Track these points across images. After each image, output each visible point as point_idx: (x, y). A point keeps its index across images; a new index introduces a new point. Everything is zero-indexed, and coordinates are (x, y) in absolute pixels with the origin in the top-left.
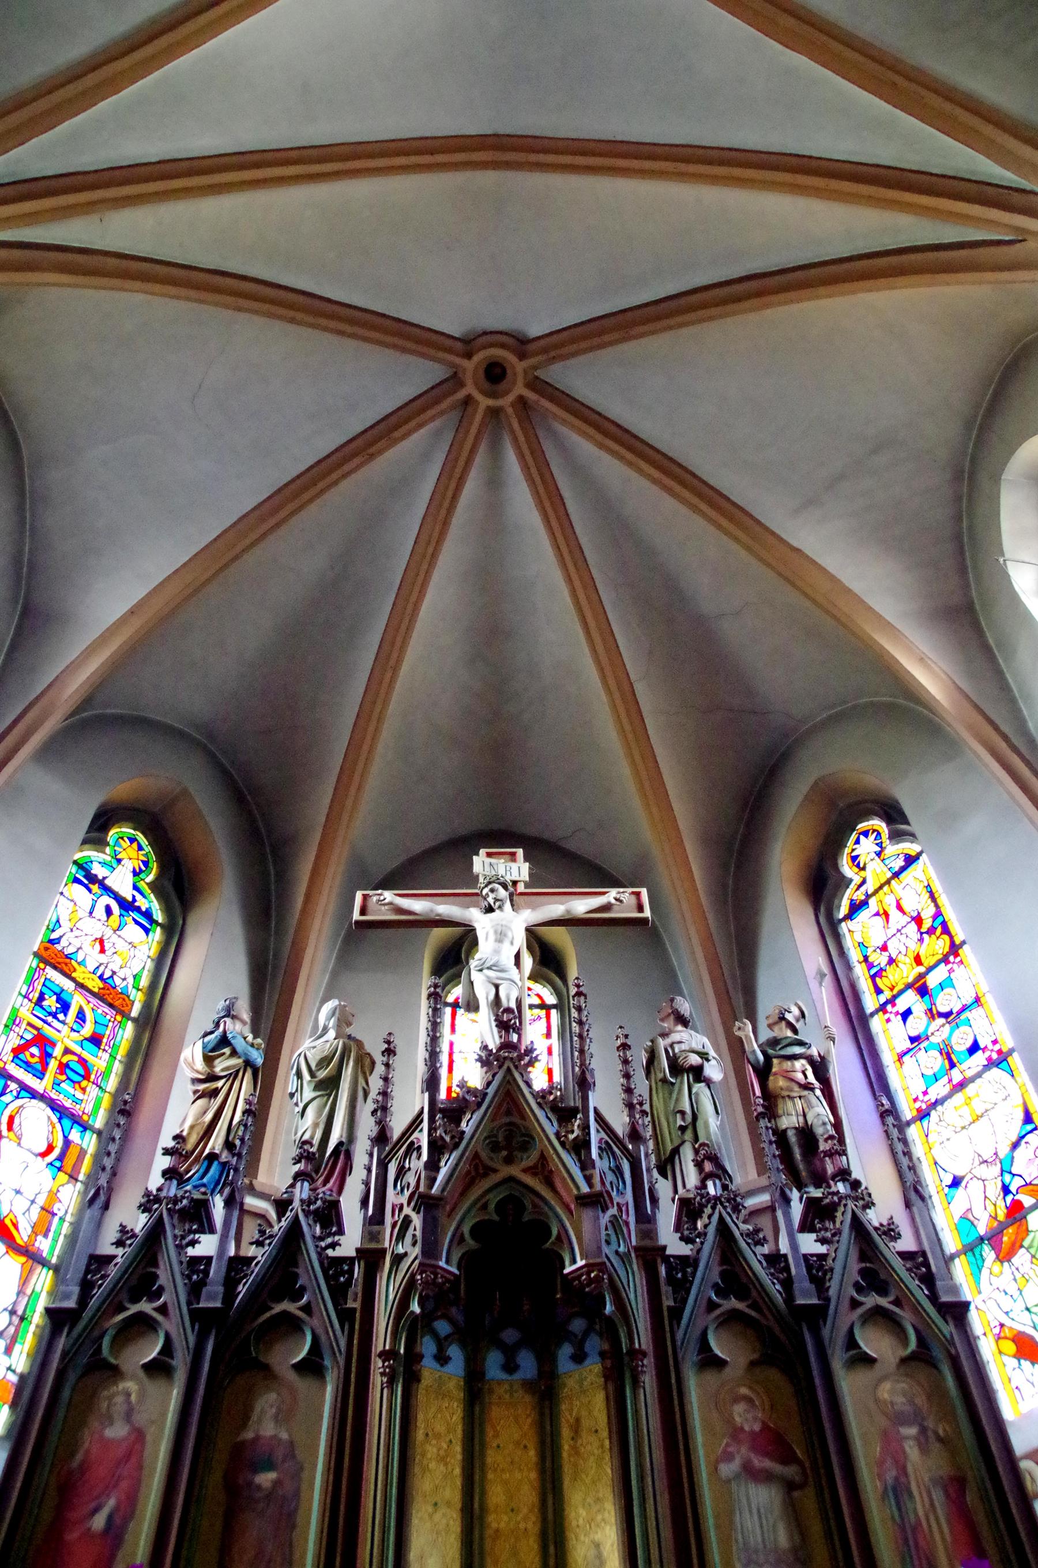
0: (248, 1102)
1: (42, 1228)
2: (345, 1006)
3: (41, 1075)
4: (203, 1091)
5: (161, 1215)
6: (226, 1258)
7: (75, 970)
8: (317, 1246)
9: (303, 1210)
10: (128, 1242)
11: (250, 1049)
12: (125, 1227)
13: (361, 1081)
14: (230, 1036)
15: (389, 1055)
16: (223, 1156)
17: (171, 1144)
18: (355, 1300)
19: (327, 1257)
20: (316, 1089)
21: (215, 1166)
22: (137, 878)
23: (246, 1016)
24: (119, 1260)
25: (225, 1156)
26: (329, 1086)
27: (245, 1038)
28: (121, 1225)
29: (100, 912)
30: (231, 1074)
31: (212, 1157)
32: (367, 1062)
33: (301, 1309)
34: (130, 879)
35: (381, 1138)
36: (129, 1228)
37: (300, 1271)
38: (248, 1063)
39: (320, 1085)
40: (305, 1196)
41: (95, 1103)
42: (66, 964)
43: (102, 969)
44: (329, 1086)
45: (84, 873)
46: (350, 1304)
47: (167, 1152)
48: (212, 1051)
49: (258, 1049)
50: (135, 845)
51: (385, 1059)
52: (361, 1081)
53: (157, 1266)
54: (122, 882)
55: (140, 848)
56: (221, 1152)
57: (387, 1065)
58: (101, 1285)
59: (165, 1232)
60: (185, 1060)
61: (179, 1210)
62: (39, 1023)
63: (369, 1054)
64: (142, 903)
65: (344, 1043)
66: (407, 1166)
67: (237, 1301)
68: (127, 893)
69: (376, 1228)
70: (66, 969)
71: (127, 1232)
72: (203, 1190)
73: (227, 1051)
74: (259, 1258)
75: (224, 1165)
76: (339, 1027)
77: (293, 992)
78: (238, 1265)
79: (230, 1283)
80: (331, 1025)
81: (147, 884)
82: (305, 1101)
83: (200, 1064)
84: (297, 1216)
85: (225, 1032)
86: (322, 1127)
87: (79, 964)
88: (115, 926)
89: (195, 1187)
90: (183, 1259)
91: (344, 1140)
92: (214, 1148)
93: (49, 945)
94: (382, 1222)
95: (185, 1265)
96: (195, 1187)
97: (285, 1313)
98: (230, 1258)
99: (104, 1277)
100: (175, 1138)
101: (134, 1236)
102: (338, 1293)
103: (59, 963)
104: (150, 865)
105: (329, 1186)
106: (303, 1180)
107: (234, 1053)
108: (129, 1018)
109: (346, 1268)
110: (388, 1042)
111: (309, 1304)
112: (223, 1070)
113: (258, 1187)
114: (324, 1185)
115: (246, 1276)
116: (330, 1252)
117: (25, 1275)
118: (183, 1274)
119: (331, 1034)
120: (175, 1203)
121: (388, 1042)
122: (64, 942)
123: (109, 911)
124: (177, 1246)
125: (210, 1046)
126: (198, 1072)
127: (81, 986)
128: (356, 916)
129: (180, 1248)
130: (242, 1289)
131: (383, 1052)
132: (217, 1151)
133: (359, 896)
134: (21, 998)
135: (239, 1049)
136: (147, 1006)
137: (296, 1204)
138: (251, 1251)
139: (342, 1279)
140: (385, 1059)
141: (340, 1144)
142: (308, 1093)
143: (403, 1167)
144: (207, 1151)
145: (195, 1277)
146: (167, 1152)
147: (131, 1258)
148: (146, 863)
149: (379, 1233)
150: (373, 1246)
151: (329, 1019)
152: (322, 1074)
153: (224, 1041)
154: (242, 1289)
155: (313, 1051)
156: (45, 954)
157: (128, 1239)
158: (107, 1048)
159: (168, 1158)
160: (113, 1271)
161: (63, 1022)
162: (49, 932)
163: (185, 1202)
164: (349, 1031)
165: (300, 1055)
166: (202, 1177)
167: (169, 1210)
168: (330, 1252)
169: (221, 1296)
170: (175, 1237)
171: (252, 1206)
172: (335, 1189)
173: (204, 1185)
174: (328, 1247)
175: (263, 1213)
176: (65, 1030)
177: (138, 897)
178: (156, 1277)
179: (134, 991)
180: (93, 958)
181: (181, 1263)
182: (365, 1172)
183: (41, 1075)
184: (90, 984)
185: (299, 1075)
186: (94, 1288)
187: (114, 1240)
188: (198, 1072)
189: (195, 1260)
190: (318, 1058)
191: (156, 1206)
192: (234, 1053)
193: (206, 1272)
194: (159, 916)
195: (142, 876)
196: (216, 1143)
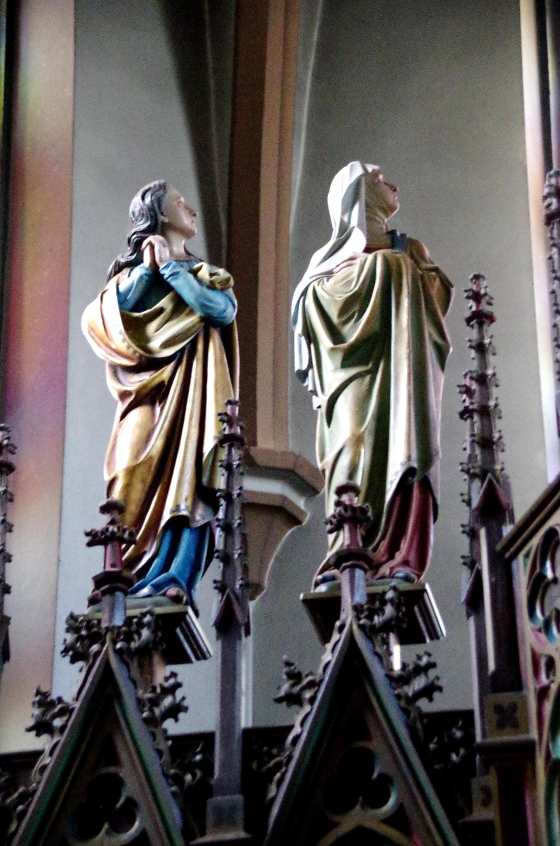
0: (224, 418)
2: (375, 174)
4: (138, 392)
5: (106, 664)
6: (238, 734)
8: (398, 697)
9: (362, 627)
11: (211, 294)
12: (45, 695)
13: (428, 329)
14: (166, 273)
15: (481, 325)
16: (198, 517)
17: (101, 522)
18: (486, 803)
19: (422, 715)
20: (345, 364)
21: (186, 538)
23: (193, 222)
24: (46, 760)
25: (201, 516)
26: (369, 354)
27: (195, 273)
28: (38, 693)
30: (182, 351)
31: (179, 523)
32: (435, 287)
33: (388, 821)
35: (492, 508)
36: (54, 696)
37: (376, 745)
38: (210, 322)
39: (350, 358)
40: (360, 598)
44: (369, 354)
46: (482, 813)
47: (95, 539)
48: (137, 307)
49: (222, 290)
51: (474, 334)
52: (428, 329)
53: (116, 761)
56: (193, 511)
57: (481, 348)
58: (24, 812)
59: (118, 695)
60: (92, 329)
61: (139, 650)
63: (436, 270)
65: (386, 261)
66: (549, 574)
67: (275, 810)
69: (506, 698)
71: (52, 704)
72: (172, 591)
73: (165, 303)
74: (297, 730)
75: (204, 532)
76: (369, 222)
77: (258, 85)
78: (263, 742)
79: (254, 783)
80: (354, 222)
82: (330, 389)
83: (119, 338)
84: (351, 638)
85: (154, 266)
86: (368, 441)
89: (157, 587)
91: (415, 465)
92: (177, 508)
94: (517, 684)
95: (166, 757)
96: (157, 587)
97: (360, 832)
98: (247, 732)
99: (26, 797)
100: (105, 509)
101: (66, 711)
102: (453, 787)
105: (399, 556)
106: (353, 567)
107: (180, 306)
109: (459, 734)
110: (477, 297)
111: (400, 809)
112: (166, 345)
113: (260, 460)
114: (391, 557)
115: (278, 767)
116: (424, 704)
118: (166, 775)
119: (358, 241)
120: (128, 638)
121: (477, 297)
124: (146, 721)
125: (132, 297)
126: (118, 353)
129: (153, 722)
130: (278, 793)
131: (469, 321)
132: (184, 513)
135: (188, 296)
137: (347, 615)
138: (280, 715)
139: (454, 757)
140: (474, 334)
141: (409, 473)
142: (334, 375)
143: (542, 576)
144: (166, 516)
145: (188, 777)
147: (68, 750)
149: (514, 707)
150: (508, 737)
151: (348, 208)
152: (353, 332)
153: (156, 284)
154: (278, 793)
155: (329, 284)
157: (54, 717)
159: (99, 549)
160: (39, 783)
163: (145, 633)
164: (387, 222)
165: (304, 293)
166: (166, 567)
167: (119, 653)
168: (424, 704)
169: (240, 815)
170: (140, 702)
171: (255, 493)
172: (412, 557)
173: (173, 581)
174: (418, 695)
175: (278, 503)
178: (118, 783)
181: (160, 753)
182: (466, 540)
185: (310, 335)
186: (10, 822)
187: (31, 722)
188: (118, 353)
189: (185, 744)
190: (341, 298)
191: (95, 648)
192: (180, 306)
193: (207, 766)
196: (179, 496)
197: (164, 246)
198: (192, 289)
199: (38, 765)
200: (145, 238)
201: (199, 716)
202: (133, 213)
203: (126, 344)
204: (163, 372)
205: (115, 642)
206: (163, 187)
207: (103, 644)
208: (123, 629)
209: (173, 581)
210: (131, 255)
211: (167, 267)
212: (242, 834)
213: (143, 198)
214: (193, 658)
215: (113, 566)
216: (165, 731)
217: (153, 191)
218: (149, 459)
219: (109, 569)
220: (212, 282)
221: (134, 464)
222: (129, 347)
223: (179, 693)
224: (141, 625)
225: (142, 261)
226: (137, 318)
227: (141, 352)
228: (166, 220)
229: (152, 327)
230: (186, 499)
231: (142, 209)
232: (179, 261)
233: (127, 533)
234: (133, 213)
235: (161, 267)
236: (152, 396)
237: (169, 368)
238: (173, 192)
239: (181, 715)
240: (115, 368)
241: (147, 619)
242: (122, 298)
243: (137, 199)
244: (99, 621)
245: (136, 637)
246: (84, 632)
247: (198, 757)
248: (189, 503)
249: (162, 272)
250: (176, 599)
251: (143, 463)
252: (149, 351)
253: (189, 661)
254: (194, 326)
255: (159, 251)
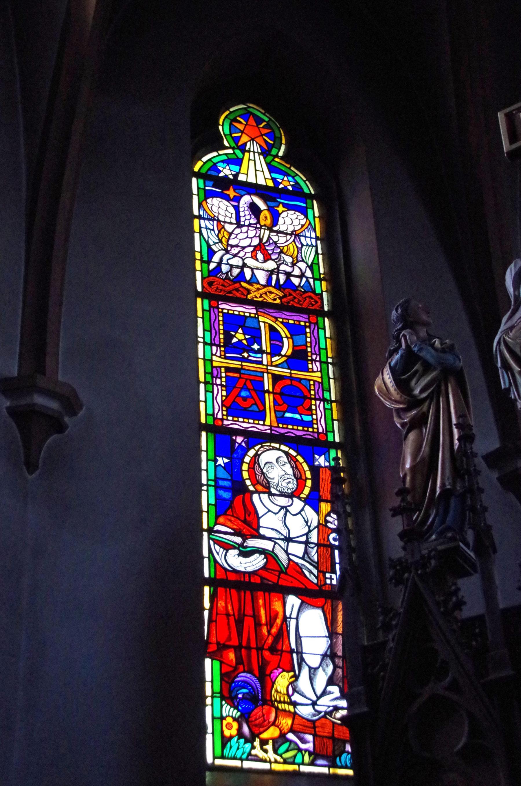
1: (324, 566)
3: (261, 416)
4: (410, 421)
7: (249, 292)
10: (394, 623)
11: (442, 355)
17: (396, 502)
22: (269, 158)
29: (246, 217)
30: (432, 392)
34: (261, 162)
41: (325, 418)
42: (237, 290)
43: (274, 277)
45: (211, 183)
50: (252, 122)
54: (255, 170)
55: (258, 121)
56: (454, 484)
62: (236, 364)
64: (286, 183)
68: (263, 178)
70: (238, 295)
81: (282, 158)
87: (249, 282)
88: (269, 222)
89: (441, 534)
90: (455, 627)
93: (211, 279)
103: (230, 292)
104: (277, 135)
108: (324, 314)
117: (329, 617)
122: (225, 268)
123: (254, 209)
127: (261, 306)
128: (506, 146)
133: (501, 116)
134: (208, 348)
136: (334, 293)
146: (396, 512)
148: (271, 135)
153: (410, 358)
156: (212, 290)
157: (391, 619)
158: (314, 357)
159: (399, 518)
161: (261, 351)
162: (205, 265)
163: (433, 562)
165: (499, 343)
166: (443, 522)
173: (449, 529)
176: (265, 359)
177: (279, 177)
179: (317, 283)
180: (260, 269)
183: (261, 416)
184: (269, 299)
188: (397, 402)
192: (427, 368)
194: (308, 188)
195: (274, 152)
197: (412, 335)
198: (432, 356)
199: (388, 648)
200: (401, 333)
201: (473, 606)
202: (393, 320)
203: (399, 396)
204: (423, 407)
205: (417, 570)
206: (407, 302)
207: (411, 572)
208: (421, 561)
209: (449, 529)
210: (396, 344)
211: (415, 346)
212: (511, 672)
213: (397, 311)
214: (473, 572)
215: (408, 526)
216: (456, 618)
217: (401, 305)
218: (423, 459)
219: (406, 528)
220: (443, 349)
221: (414, 464)
222: (401, 397)
223: (460, 594)
224: (430, 558)
225: (401, 346)
226: (404, 379)
227: (408, 398)
228: (411, 319)
229: (413, 383)
230: (448, 479)
231: (397, 317)
232: (423, 341)
233: (413, 505)
234: (393, 320)
235: (413, 346)
236: (418, 423)
237: (427, 404)
238: (413, 303)
239: (464, 608)
240: (398, 410)
241: (433, 553)
242: (393, 370)
243: (394, 312)
244: (407, 560)
245: (428, 565)
246: (398, 568)
247: (477, 630)
248: (450, 481)
249: (413, 349)
250: (452, 539)
251: (420, 461)
252: (414, 397)
253: (471, 574)
254: (437, 377)
255: (410, 338)
